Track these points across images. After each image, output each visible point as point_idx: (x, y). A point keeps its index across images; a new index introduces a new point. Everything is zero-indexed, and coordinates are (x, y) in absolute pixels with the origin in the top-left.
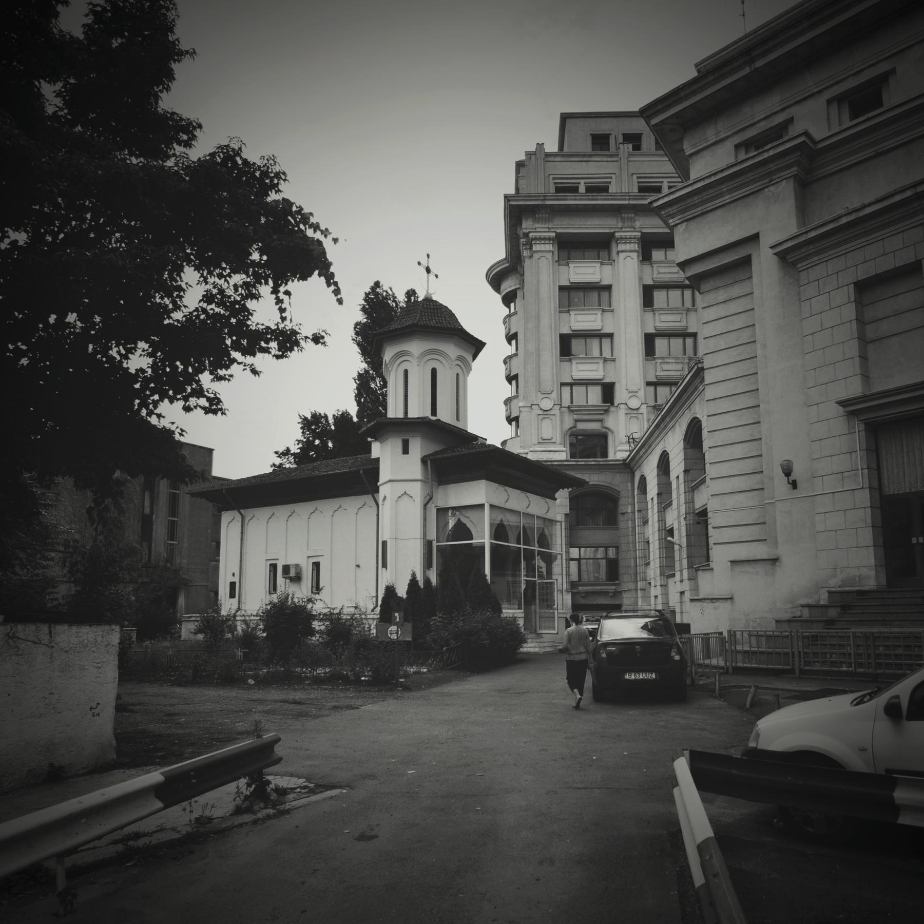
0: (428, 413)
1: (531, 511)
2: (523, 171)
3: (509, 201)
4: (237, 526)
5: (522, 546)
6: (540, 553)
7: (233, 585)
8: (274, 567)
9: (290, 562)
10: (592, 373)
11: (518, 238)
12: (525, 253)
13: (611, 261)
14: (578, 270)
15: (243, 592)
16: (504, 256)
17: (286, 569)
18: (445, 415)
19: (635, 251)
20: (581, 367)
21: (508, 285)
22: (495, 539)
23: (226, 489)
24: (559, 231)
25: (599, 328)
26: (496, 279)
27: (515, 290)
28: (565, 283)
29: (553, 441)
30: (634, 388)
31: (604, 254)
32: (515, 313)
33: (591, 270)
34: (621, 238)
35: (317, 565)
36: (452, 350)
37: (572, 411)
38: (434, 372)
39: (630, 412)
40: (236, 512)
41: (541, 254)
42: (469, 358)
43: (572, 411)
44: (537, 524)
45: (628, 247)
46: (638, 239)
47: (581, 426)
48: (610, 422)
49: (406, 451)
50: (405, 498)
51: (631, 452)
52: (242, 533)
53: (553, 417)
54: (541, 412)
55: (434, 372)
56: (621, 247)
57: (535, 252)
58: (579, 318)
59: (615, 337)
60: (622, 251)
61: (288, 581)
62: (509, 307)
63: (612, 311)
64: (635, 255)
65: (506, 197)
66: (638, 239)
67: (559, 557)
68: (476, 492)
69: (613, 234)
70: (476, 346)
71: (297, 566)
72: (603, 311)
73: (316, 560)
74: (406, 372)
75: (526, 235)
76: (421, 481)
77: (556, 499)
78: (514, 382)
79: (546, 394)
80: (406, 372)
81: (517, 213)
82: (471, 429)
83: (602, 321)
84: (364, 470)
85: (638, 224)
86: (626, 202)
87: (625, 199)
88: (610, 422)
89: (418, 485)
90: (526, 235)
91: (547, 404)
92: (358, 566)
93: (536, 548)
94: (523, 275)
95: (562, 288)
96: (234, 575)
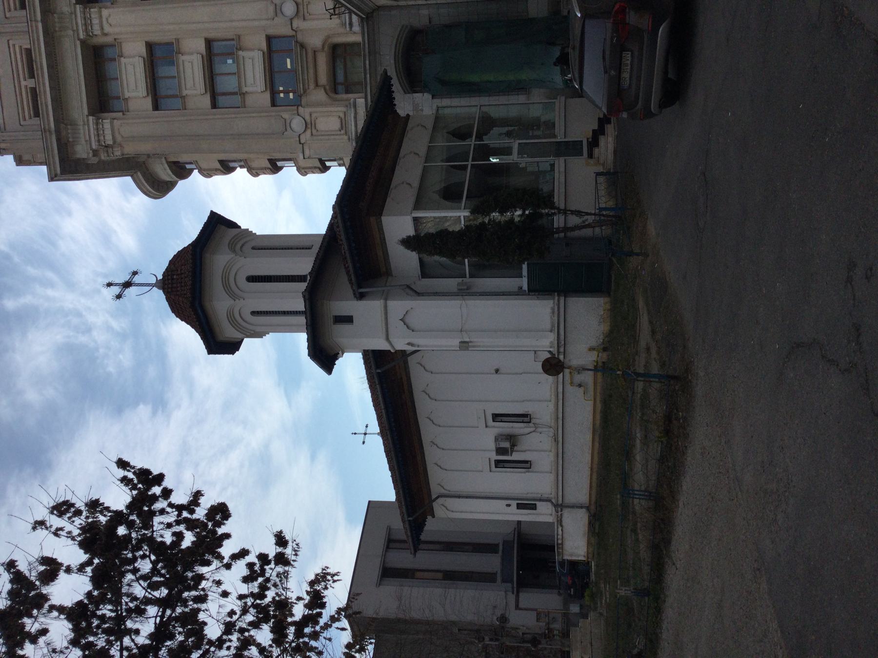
0: (303, 286)
1: (423, 152)
2: (26, 157)
3: (56, 175)
4: (450, 502)
5: (470, 163)
6: (479, 137)
7: (519, 506)
8: (498, 463)
9: (492, 446)
10: (257, 65)
11: (101, 162)
12: (118, 153)
13: (116, 44)
14: (132, 86)
15: (530, 496)
16: (129, 179)
17: (500, 451)
18: (304, 265)
19: (100, 12)
20: (250, 80)
21: (164, 173)
22: (461, 198)
23: (409, 516)
24: (86, 112)
25: (200, 56)
26: (157, 187)
27: (168, 163)
28: (148, 103)
29: (342, 115)
30: (271, 8)
31: (109, 53)
32: (196, 163)
33: (130, 68)
34: (86, 30)
35: (496, 417)
36: (220, 260)
37: (305, 92)
38: (252, 279)
39: (301, 14)
40: (434, 504)
41: (117, 135)
42: (234, 231)
43: (305, 92)
44: (441, 142)
45: (96, 21)
46: (85, 8)
47: (323, 79)
48: (315, 41)
49: (349, 320)
50: (407, 320)
51: (351, 12)
52: (459, 497)
53: (314, 115)
54: (309, 132)
55: (252, 279)
56: (97, 30)
57: (115, 142)
58: (190, 84)
59: (212, 35)
60: (102, 28)
61: (515, 448)
62: (191, 171)
63: (178, 40)
64: (105, 13)
65: (52, 178)
66: (85, 8)
67: (484, 109)
68: (397, 225)
69: (83, 43)
70: (216, 224)
71: (496, 439)
72: (179, 52)
73: (490, 418)
74: (254, 313)
75: (95, 153)
76: (386, 299)
77: (408, 115)
78: (279, 164)
79: (287, 125)
80: (254, 313)
81: (69, 167)
82: (323, 230)
83: (192, 54)
84: (377, 367)
85: (66, 9)
86: (40, 25)
87: (37, 27)
88: (315, 41)
89: (391, 304)
90: (95, 153)
91: (297, 124)
92: (497, 371)
93: (472, 142)
94: (149, 156)
95: (156, 107)
96: (509, 505)
